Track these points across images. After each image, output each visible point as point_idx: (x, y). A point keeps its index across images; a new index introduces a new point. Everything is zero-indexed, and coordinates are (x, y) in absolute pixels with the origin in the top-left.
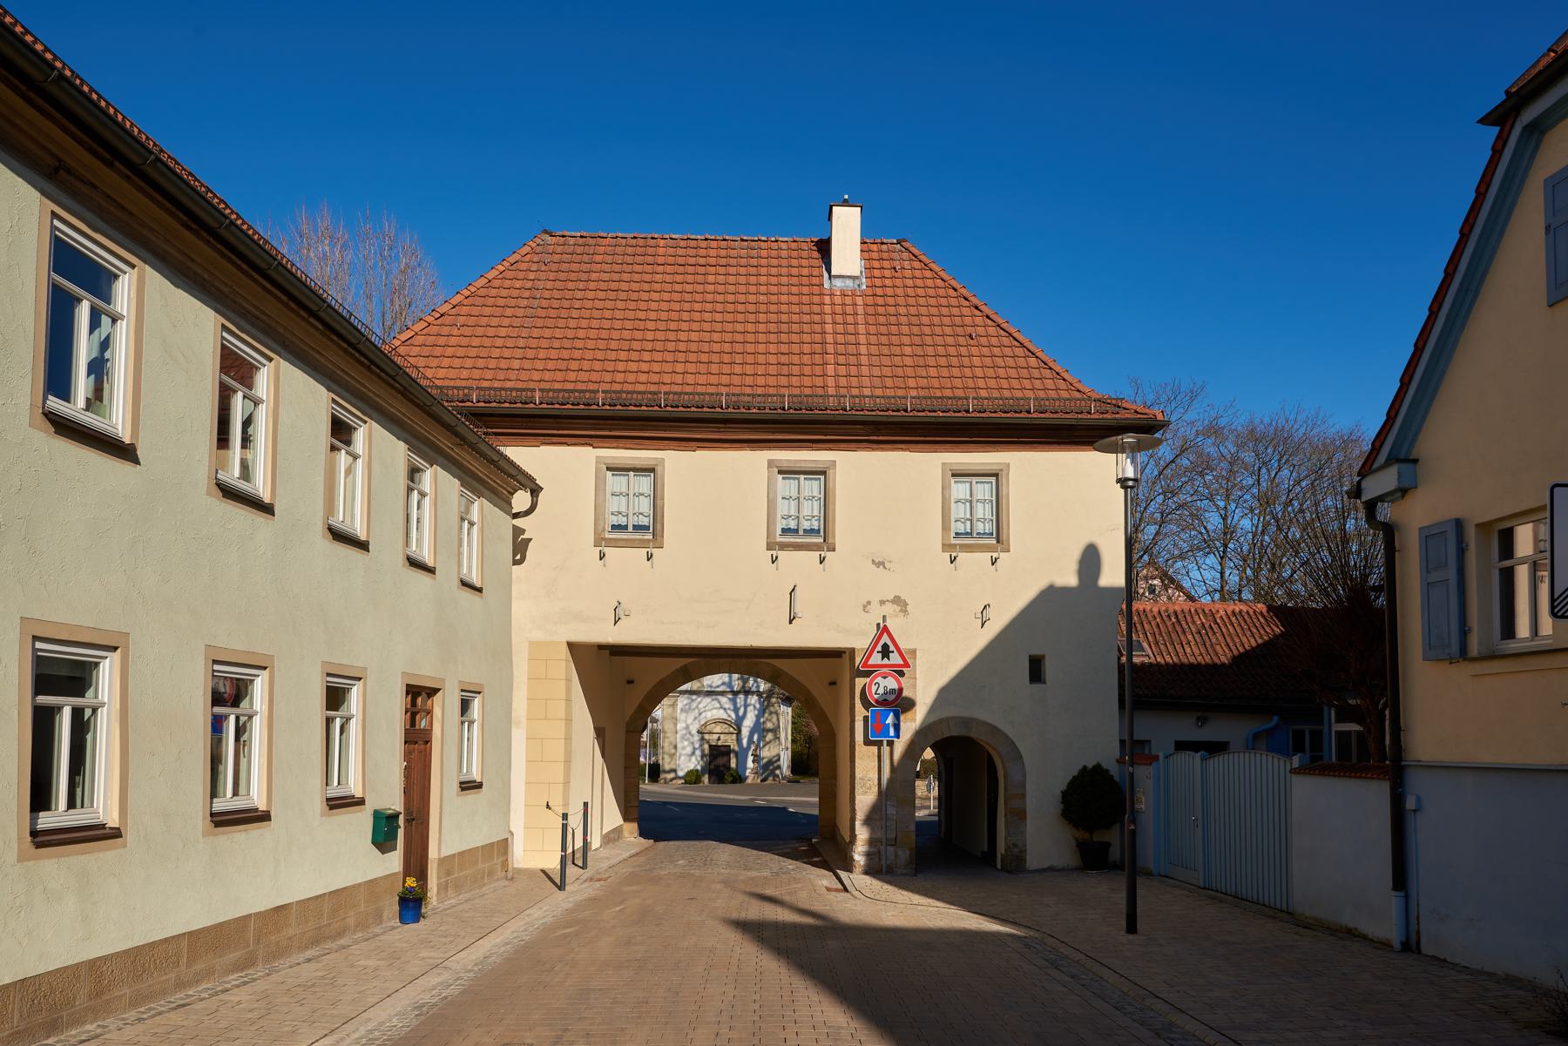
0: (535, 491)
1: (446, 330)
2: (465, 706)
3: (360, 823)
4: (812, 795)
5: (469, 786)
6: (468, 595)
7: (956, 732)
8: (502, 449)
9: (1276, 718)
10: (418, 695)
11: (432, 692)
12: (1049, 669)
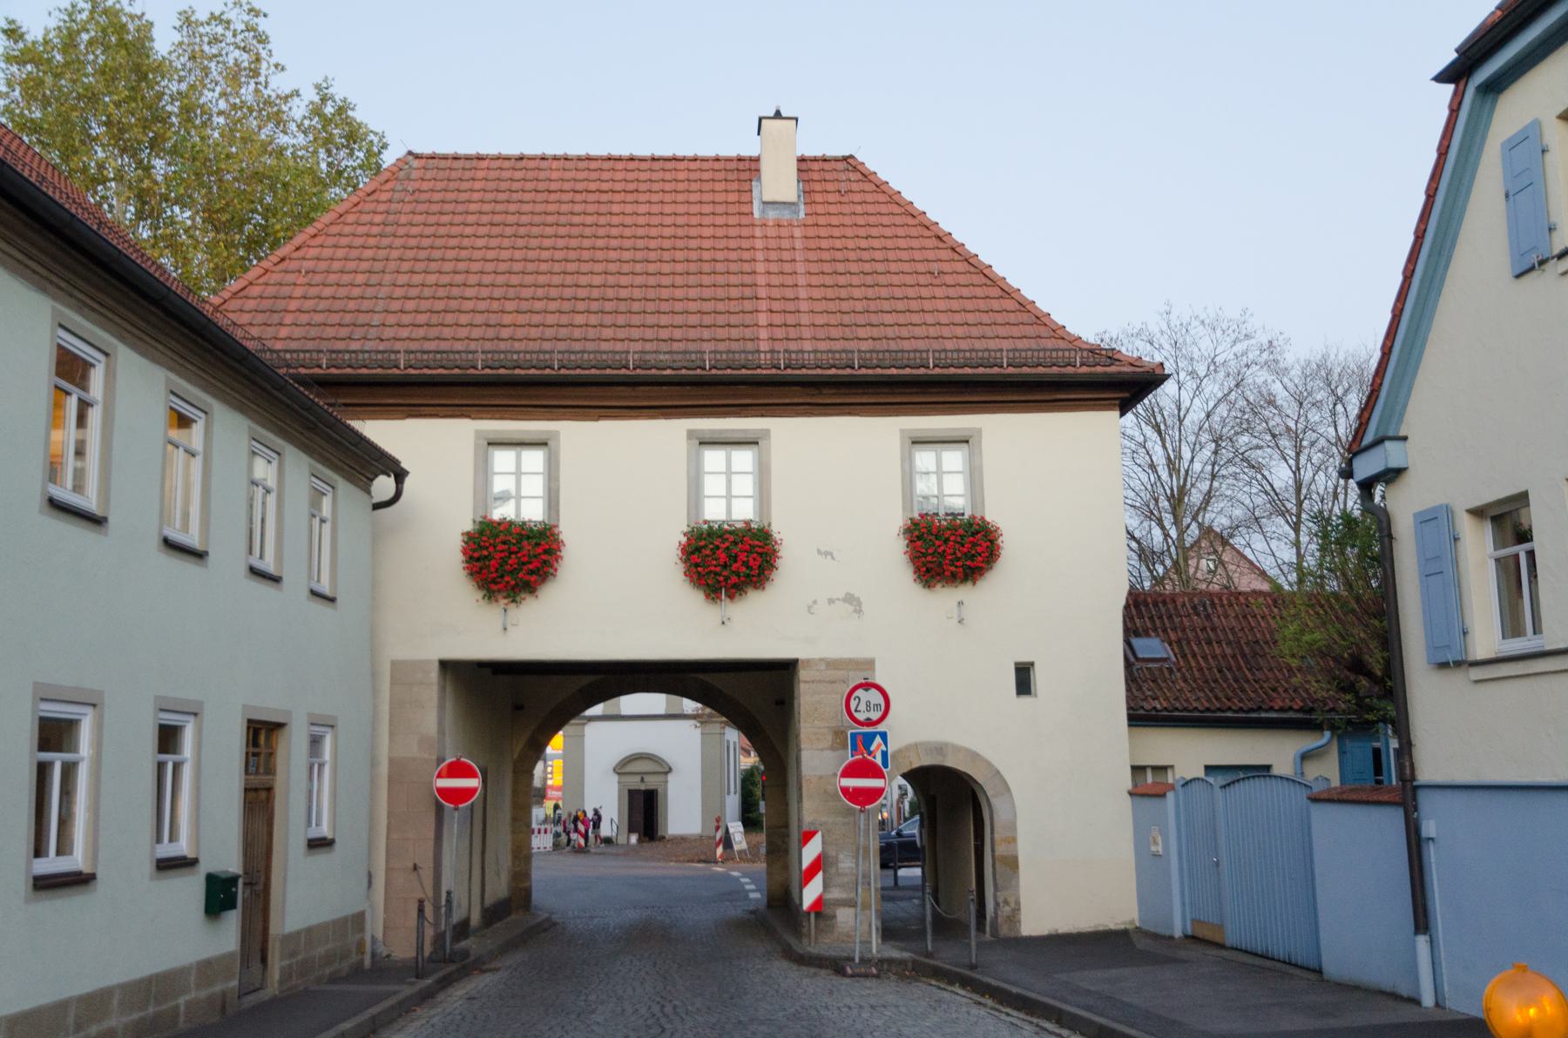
0: (400, 476)
1: (290, 278)
2: (316, 741)
3: (191, 888)
4: (905, 878)
5: (319, 844)
6: (319, 607)
7: (927, 761)
8: (356, 424)
9: (1327, 734)
10: (261, 735)
11: (278, 726)
12: (1039, 678)
